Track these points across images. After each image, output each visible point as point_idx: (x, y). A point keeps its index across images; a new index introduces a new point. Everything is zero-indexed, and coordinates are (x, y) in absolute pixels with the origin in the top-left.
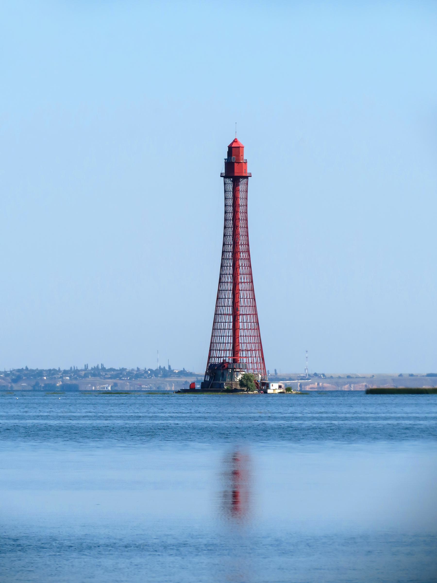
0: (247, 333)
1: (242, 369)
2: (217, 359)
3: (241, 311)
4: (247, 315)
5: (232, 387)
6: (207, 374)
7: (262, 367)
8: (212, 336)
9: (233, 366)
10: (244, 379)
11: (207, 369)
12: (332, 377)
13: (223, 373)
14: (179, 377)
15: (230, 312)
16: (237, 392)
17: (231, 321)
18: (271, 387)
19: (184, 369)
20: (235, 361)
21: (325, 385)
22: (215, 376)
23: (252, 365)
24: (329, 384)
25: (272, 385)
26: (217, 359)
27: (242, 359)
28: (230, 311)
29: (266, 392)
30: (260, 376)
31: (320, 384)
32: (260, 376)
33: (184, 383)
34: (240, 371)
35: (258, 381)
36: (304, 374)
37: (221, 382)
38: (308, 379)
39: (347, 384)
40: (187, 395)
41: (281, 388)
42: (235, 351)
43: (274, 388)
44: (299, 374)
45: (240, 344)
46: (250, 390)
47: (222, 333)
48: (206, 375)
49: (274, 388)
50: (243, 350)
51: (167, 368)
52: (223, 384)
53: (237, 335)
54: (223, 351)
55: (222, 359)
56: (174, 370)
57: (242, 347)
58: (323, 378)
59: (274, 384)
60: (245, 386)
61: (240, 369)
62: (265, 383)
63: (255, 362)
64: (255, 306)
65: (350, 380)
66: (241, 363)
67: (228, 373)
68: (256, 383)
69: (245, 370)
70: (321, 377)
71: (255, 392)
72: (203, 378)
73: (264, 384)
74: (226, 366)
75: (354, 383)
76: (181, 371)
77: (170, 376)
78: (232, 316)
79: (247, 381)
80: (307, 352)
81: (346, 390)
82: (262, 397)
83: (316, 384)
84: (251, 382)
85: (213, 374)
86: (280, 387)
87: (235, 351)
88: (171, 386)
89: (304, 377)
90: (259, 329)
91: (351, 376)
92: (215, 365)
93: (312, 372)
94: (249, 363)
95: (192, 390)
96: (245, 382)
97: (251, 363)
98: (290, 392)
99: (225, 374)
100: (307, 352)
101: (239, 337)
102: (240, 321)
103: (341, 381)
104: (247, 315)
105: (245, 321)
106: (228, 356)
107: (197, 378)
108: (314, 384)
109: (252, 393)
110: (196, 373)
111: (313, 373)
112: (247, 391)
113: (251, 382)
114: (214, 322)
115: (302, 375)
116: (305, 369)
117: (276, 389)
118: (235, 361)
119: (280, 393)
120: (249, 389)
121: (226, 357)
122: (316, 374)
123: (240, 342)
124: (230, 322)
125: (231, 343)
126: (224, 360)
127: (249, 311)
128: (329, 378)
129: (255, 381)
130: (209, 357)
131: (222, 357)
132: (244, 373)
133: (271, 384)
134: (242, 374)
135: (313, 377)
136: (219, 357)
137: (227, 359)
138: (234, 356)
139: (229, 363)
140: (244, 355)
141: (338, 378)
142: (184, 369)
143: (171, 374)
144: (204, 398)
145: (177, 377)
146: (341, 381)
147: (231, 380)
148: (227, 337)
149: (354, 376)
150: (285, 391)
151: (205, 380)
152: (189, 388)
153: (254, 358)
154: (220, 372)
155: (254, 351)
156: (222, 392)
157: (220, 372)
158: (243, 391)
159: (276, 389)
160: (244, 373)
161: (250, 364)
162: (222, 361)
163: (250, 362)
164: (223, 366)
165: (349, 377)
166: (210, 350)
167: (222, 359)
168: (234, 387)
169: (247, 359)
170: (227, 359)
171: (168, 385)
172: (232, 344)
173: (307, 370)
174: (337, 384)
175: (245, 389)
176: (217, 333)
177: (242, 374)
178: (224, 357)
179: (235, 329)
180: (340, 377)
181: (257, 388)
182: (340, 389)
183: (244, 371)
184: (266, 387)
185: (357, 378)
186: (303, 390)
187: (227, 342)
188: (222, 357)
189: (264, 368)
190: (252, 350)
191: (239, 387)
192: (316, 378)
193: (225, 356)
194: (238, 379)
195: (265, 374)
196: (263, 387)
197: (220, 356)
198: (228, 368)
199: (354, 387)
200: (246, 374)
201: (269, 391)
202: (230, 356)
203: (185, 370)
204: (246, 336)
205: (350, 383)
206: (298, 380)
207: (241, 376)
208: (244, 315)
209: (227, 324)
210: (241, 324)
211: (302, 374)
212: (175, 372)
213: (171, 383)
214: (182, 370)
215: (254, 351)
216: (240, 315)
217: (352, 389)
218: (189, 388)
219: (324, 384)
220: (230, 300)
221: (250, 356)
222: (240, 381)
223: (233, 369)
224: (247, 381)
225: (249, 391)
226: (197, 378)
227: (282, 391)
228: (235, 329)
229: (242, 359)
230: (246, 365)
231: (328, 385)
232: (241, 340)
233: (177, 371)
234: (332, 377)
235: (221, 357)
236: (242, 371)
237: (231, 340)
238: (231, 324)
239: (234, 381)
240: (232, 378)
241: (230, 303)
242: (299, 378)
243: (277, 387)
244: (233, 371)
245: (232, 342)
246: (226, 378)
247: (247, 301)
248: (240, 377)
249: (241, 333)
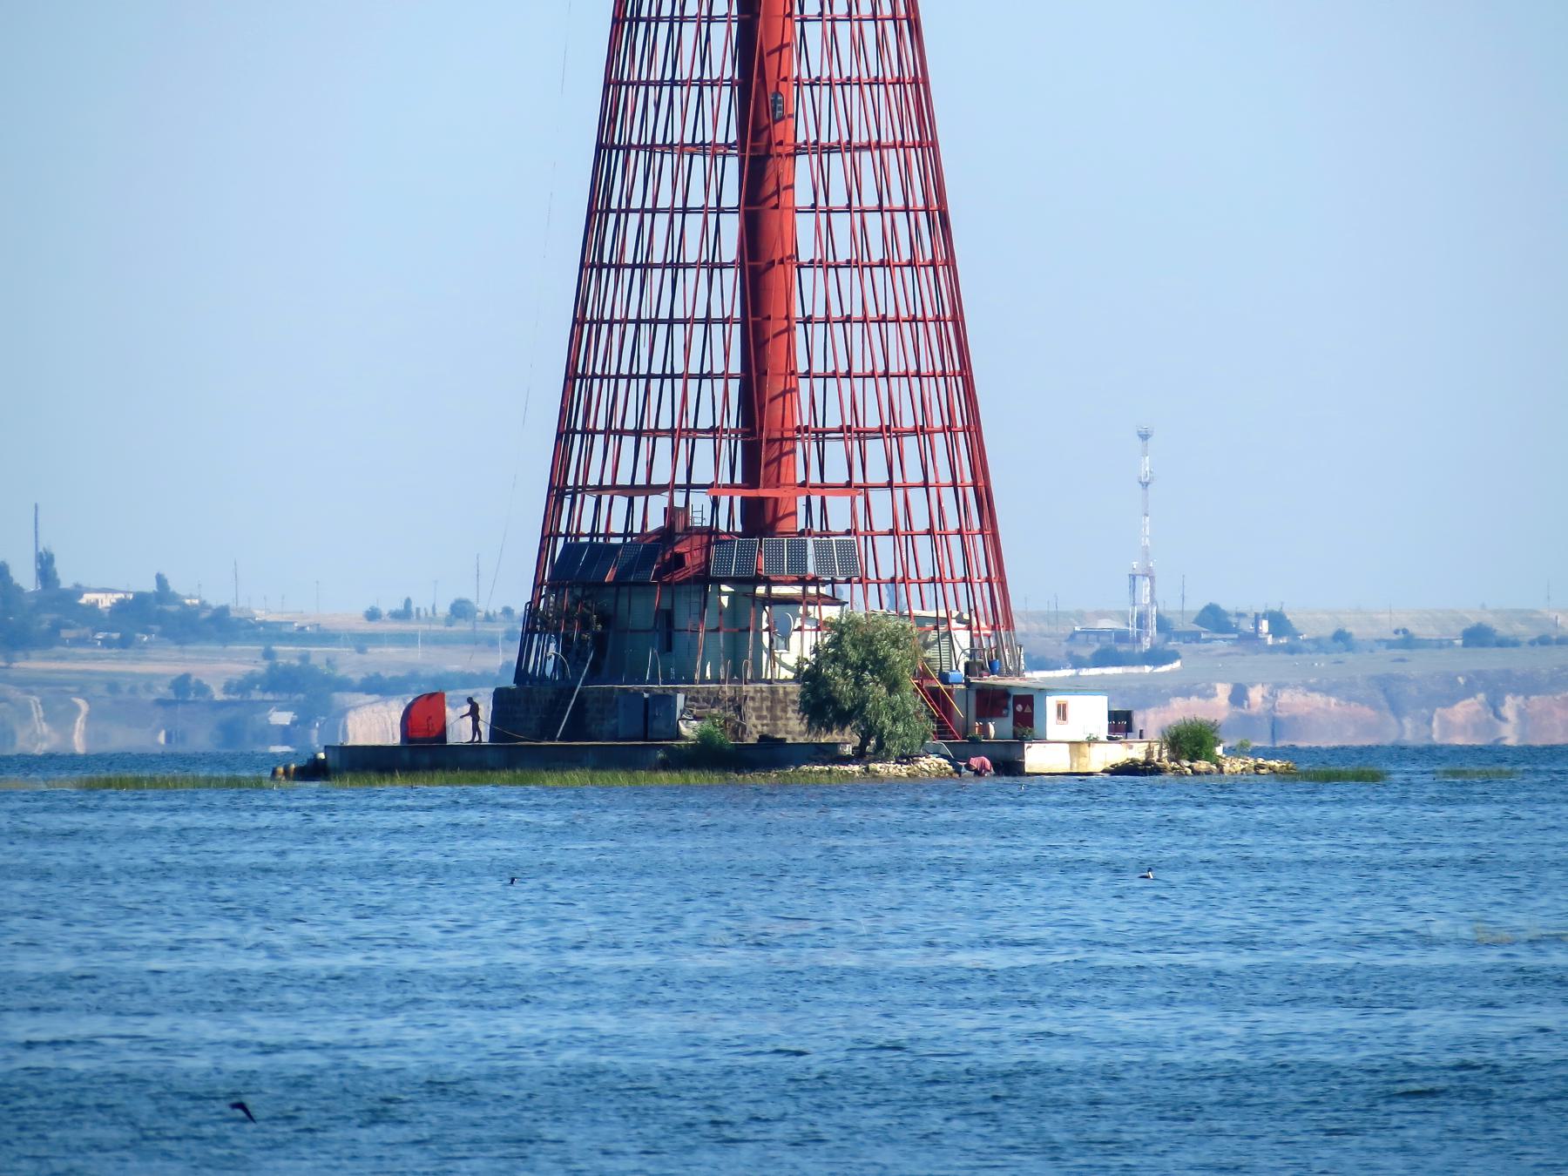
0: (851, 292)
1: (815, 581)
2: (621, 502)
3: (811, 115)
4: (849, 147)
5: (739, 730)
6: (535, 623)
7: (980, 569)
8: (578, 322)
9: (748, 557)
10: (835, 658)
11: (537, 585)
12: (1341, 637)
13: (666, 619)
14: (125, 643)
15: (725, 129)
16: (779, 763)
17: (731, 198)
18: (1053, 728)
19: (161, 580)
20: (760, 519)
21: (1293, 701)
22: (600, 642)
23: (935, 548)
24: (1328, 692)
25: (1062, 711)
26: (621, 502)
27: (816, 501)
28: (719, 118)
29: (1010, 766)
30: (962, 638)
31: (1256, 695)
32: (962, 638)
33: (162, 690)
34: (804, 600)
35: (944, 678)
36: (1123, 616)
37: (658, 687)
38: (1156, 657)
39: (1469, 691)
40: (393, 790)
41: (1129, 729)
42: (760, 438)
43: (1075, 729)
44: (1081, 616)
45: (804, 384)
46: (880, 745)
47: (656, 295)
48: (529, 632)
49: (1073, 734)
50: (821, 435)
51: (25, 577)
52: (667, 700)
53: (776, 309)
54: (664, 444)
55: (658, 503)
56: (79, 591)
57: (817, 402)
58: (1273, 649)
59: (1075, 703)
60: (843, 719)
61: (803, 582)
62: (1004, 693)
63: (921, 524)
64: (921, 82)
65: (1489, 660)
66: (806, 532)
67: (710, 619)
68: (935, 694)
69: (844, 591)
70: (1254, 636)
71: (931, 763)
72: (507, 656)
73: (991, 702)
74: (693, 561)
75: (1527, 686)
76: (141, 598)
77: (49, 640)
78: (733, 164)
79: (859, 683)
80: (1144, 437)
81: (1459, 741)
82: (998, 804)
83: (1223, 691)
84: (893, 686)
85: (586, 625)
86: (1121, 724)
87: (760, 438)
88: (61, 717)
89: (1122, 637)
90: (950, 262)
91: (1502, 630)
92: (601, 552)
93: (1182, 599)
94: (871, 533)
95: (422, 751)
96: (843, 687)
97: (930, 532)
98: (1202, 765)
99: (683, 619)
100: (1144, 437)
101: (789, 330)
102: (803, 196)
103: (1418, 666)
104: (849, 147)
105: (838, 199)
106: (701, 482)
107: (268, 655)
108: (1207, 694)
109: (904, 770)
110: (260, 615)
111: (1196, 605)
112: (860, 756)
113: (893, 686)
114: (597, 211)
115: (1104, 624)
116: (1133, 577)
117: (1092, 741)
118: (760, 519)
119: (1129, 769)
120: (874, 746)
121: (689, 487)
122: (1214, 619)
123: (802, 367)
124: (720, 210)
125: (726, 376)
126: (670, 512)
127: (871, 114)
128: (1318, 644)
129: (924, 675)
130: (558, 492)
131: (660, 489)
132: (831, 612)
133: (1051, 702)
134: (820, 626)
135: (1195, 637)
136: (631, 491)
137: (700, 501)
138: (751, 479)
139: (711, 532)
140: (836, 473)
141: (1391, 645)
142: (161, 580)
143: (56, 627)
144: (513, 820)
145: (107, 643)
146: (1418, 666)
147: (736, 673)
148: (662, 329)
149: (1524, 631)
150: (1161, 756)
151: (521, 674)
152: (395, 739)
153: (917, 496)
154: (641, 610)
155: (910, 443)
156: (665, 765)
157: (641, 610)
158: (829, 754)
159: (1092, 741)
160: (831, 612)
161: (885, 544)
162: (656, 521)
163: (882, 522)
164: (664, 559)
165: (1477, 636)
166: (565, 434)
167: (658, 503)
168: (755, 727)
169: (860, 501)
170: (700, 501)
171: (38, 713)
172: (734, 385)
173: (1144, 587)
174: (1390, 694)
175: (847, 739)
176: (617, 297)
177: (820, 626)
178: (671, 487)
179: (761, 264)
180: (1407, 641)
181: (942, 732)
182: (1409, 732)
183: (833, 601)
184: (1007, 724)
185: (1544, 641)
186: (350, 743)
187: (694, 369)
188: (660, 489)
189: (998, 578)
190: (900, 434)
191: (793, 728)
192: (1221, 644)
193: (681, 479)
194: (790, 658)
195: (1002, 617)
196: (988, 722)
197: (641, 480)
198: (705, 580)
199: (1521, 713)
200: (854, 624)
201: (1036, 758)
202: (725, 479)
203: (175, 586)
204: (914, 319)
205: (1494, 689)
206: (1078, 663)
207: (810, 638)
208: (830, 149)
209: (694, 221)
210: (805, 227)
211: (1102, 615)
212: (93, 606)
213: (58, 693)
214: (150, 587)
215: (910, 443)
216: (798, 150)
217: (1510, 736)
218: (395, 739)
219: (1285, 697)
220: (718, 31)
221: (877, 474)
222: (810, 678)
223: (746, 581)
224: (859, 683)
225: (881, 754)
226: (268, 655)
227: (1137, 752)
228: (761, 264)
229: (816, 501)
230: (848, 552)
231: (1318, 699)
232: (809, 348)
233: (106, 601)
234: (1341, 637)
235: (650, 489)
236: (820, 600)
237: (724, 351)
238: (731, 226)
239: (757, 678)
240: (739, 655)
241: (722, 62)
242: (1086, 653)
243: (1101, 728)
244: (748, 603)
245: (735, 367)
246: (691, 651)
247: (858, 45)
248: (801, 647)
249: (811, 292)
